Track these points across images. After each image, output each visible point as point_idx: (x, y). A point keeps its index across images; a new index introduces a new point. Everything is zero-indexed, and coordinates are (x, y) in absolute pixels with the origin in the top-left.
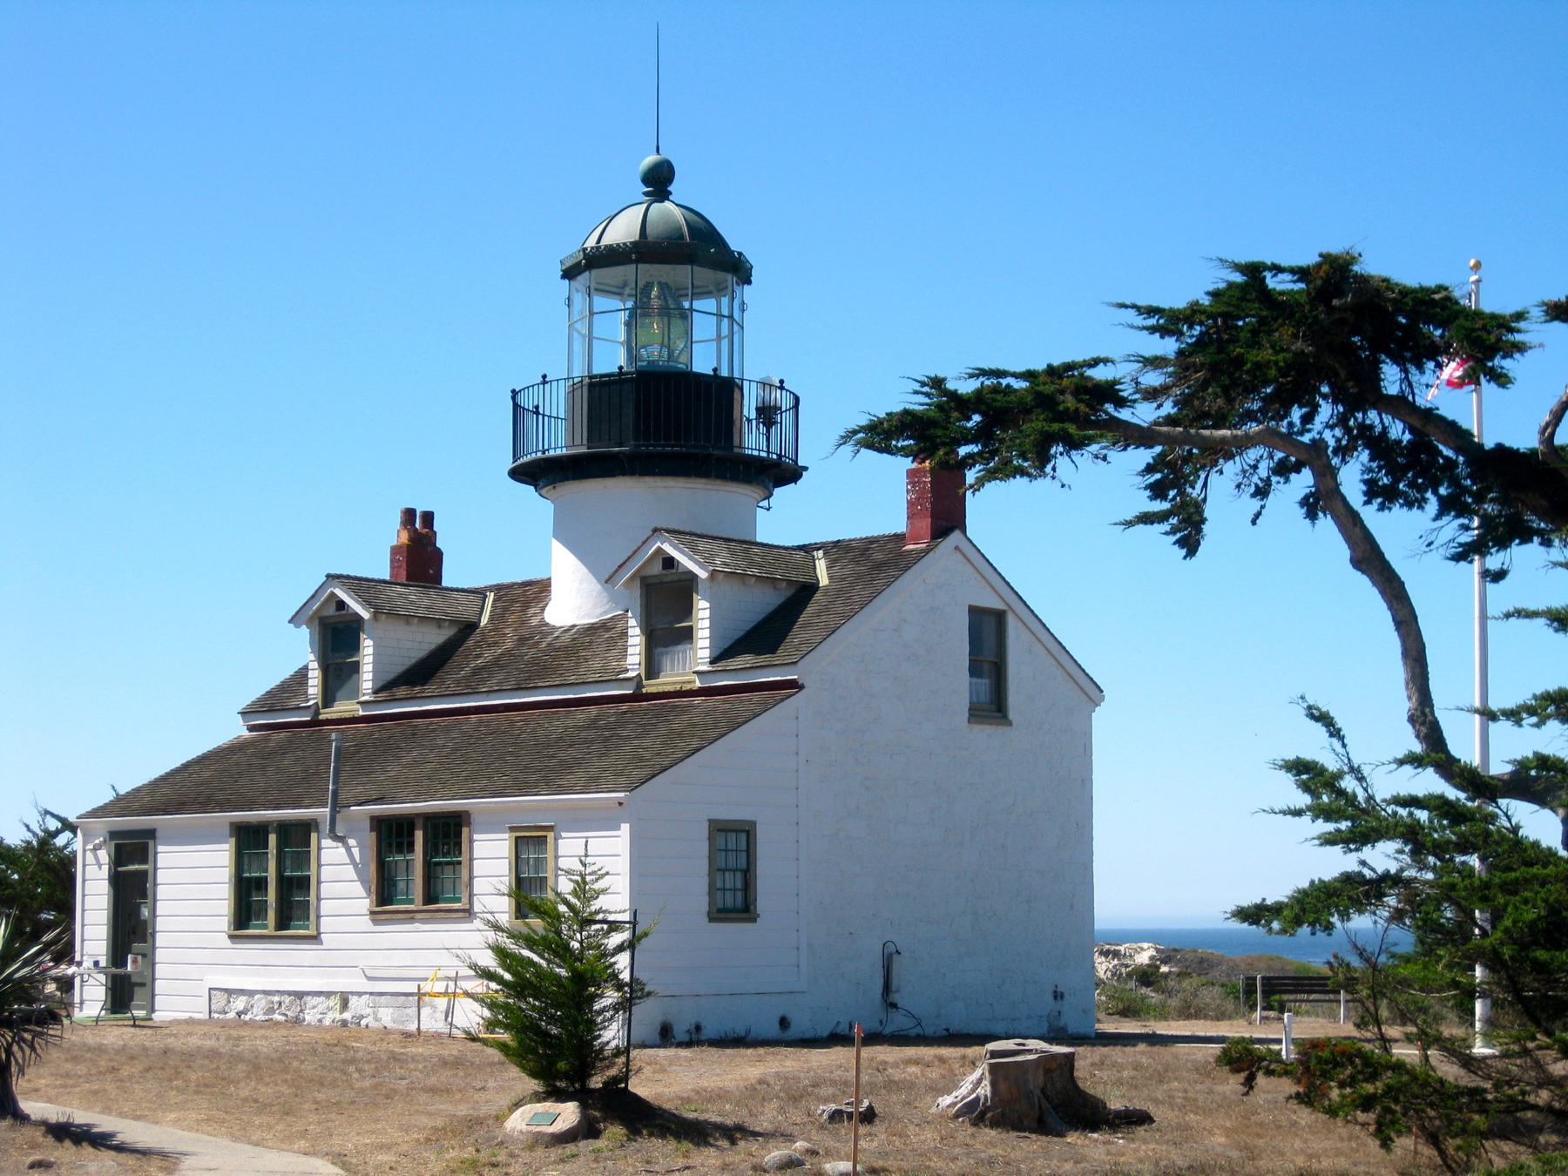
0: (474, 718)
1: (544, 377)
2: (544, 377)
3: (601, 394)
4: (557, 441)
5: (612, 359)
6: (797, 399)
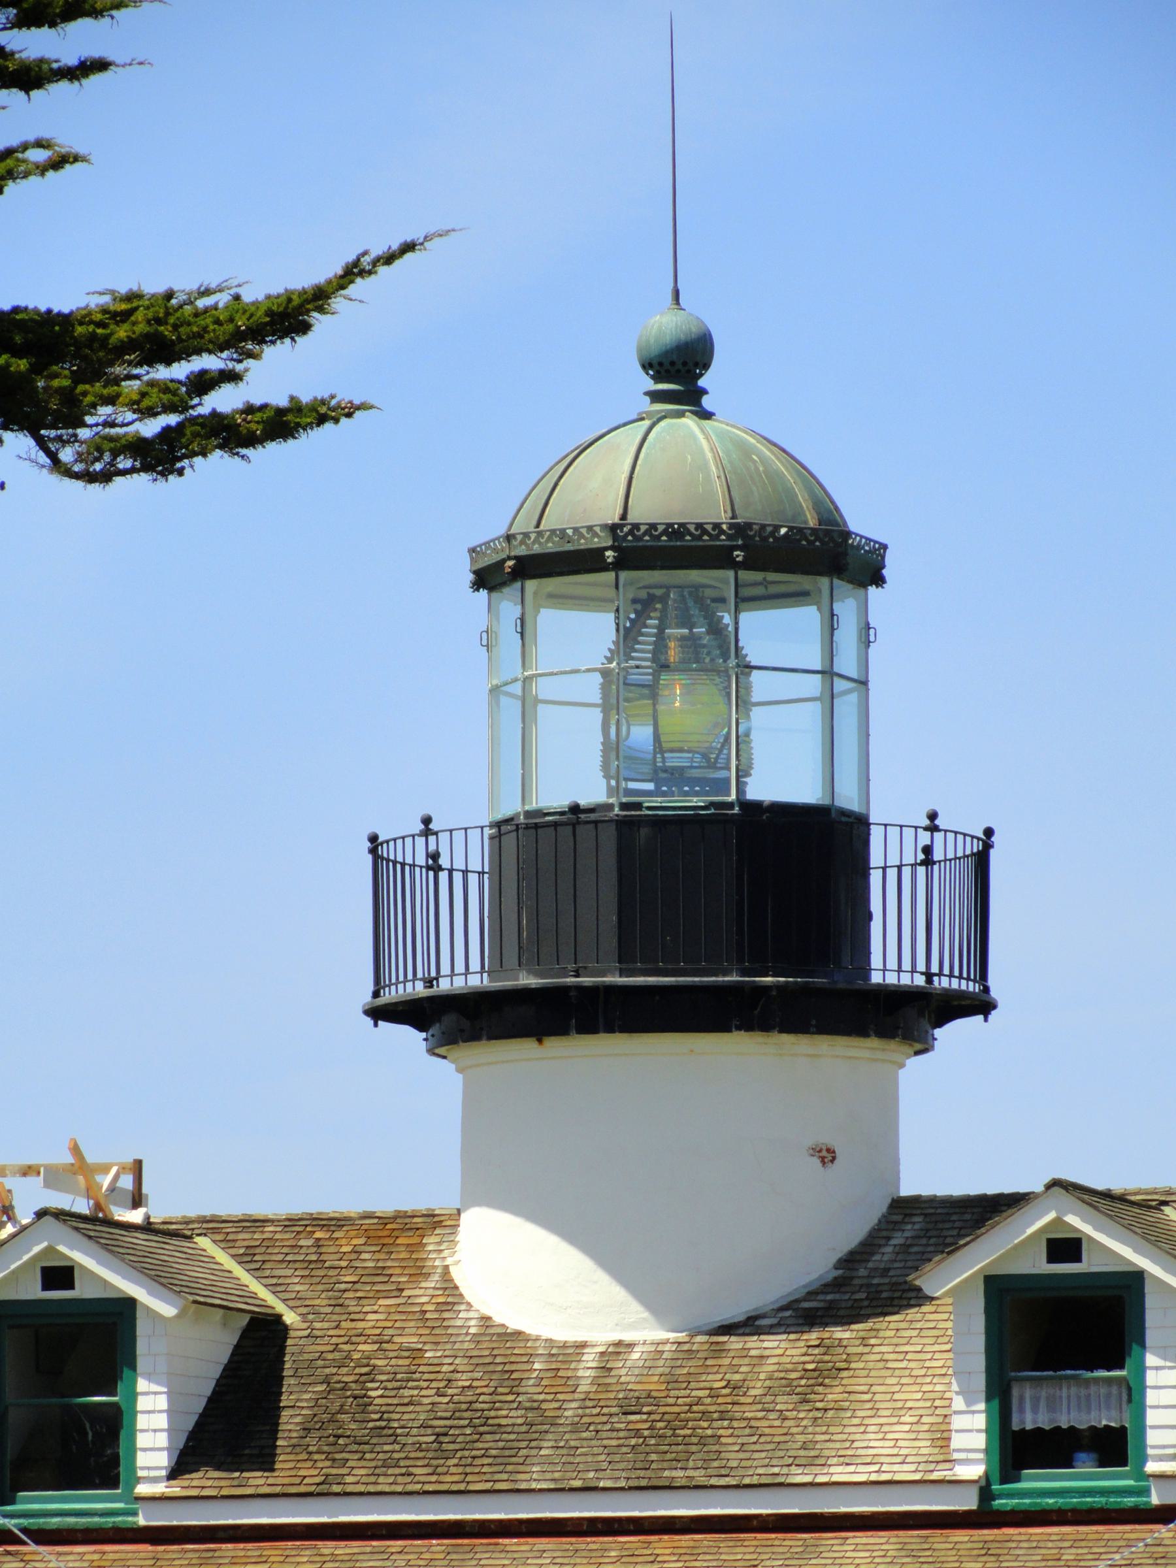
1: (427, 821)
5: (574, 774)
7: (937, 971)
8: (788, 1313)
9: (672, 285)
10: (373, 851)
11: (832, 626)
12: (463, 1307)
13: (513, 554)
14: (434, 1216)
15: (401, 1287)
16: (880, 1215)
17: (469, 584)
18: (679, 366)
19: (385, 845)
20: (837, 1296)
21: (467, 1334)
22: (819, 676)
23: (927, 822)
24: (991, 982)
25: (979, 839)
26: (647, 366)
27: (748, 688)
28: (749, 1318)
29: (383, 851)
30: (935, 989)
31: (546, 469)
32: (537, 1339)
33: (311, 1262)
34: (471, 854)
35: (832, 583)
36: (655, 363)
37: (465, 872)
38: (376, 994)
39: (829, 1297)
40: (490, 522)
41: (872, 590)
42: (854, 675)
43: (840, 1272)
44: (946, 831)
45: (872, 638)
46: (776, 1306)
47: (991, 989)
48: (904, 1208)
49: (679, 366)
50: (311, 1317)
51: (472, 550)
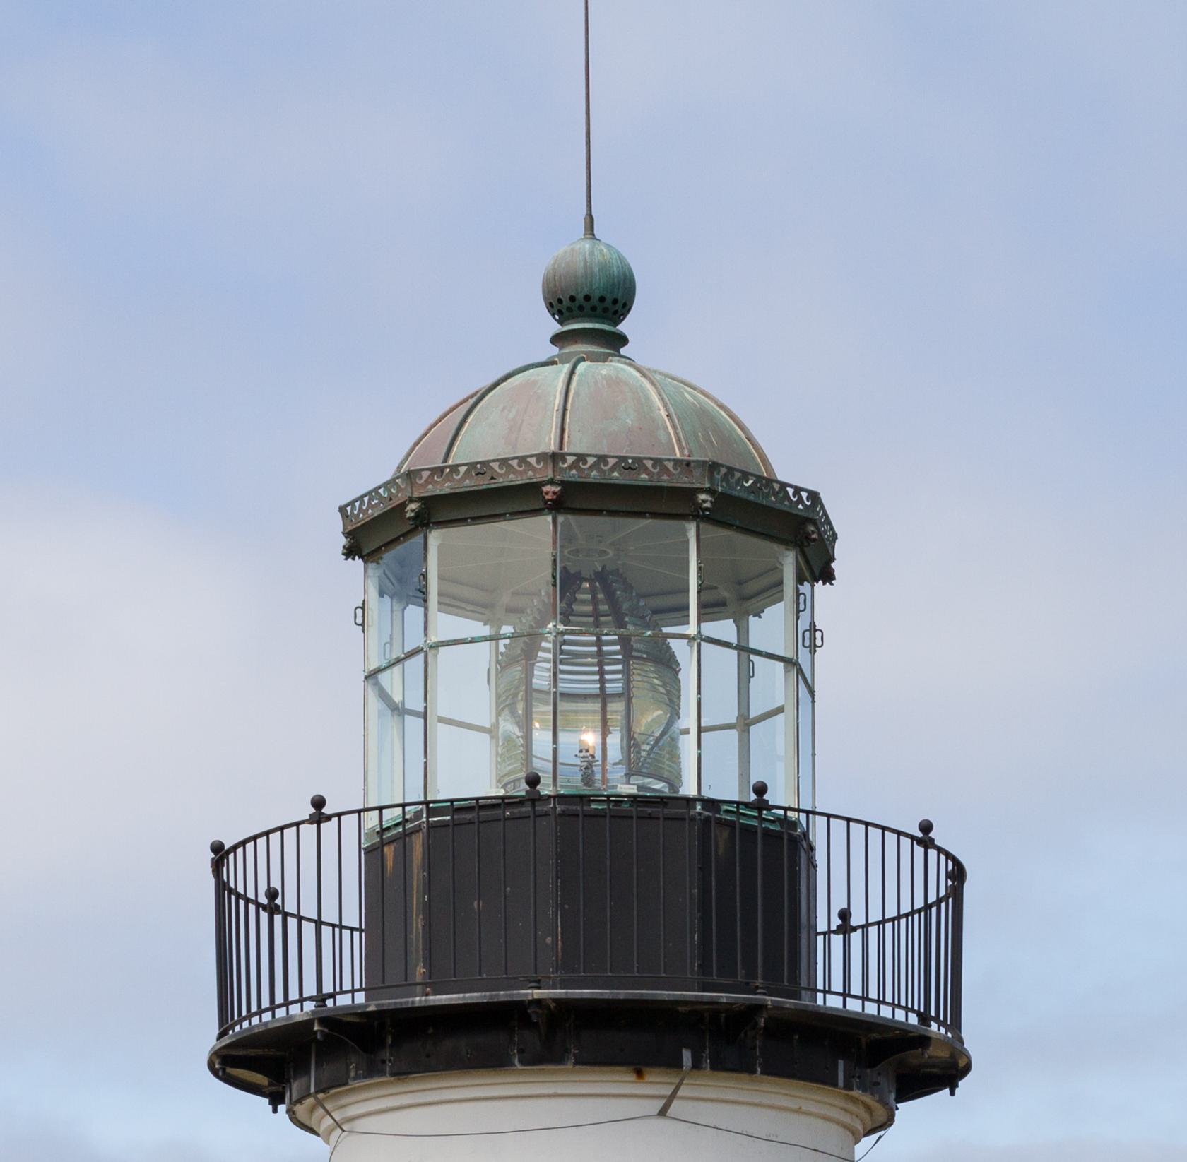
0: (759, 530)
1: (319, 803)
2: (319, 803)
3: (440, 862)
4: (327, 970)
5: (470, 771)
6: (958, 874)
9: (584, 212)
13: (416, 495)
18: (594, 302)
22: (782, 664)
24: (965, 1033)
31: (446, 408)
37: (319, 923)
38: (222, 1035)
40: (371, 463)
41: (819, 586)
45: (818, 642)
49: (608, 303)
51: (342, 510)
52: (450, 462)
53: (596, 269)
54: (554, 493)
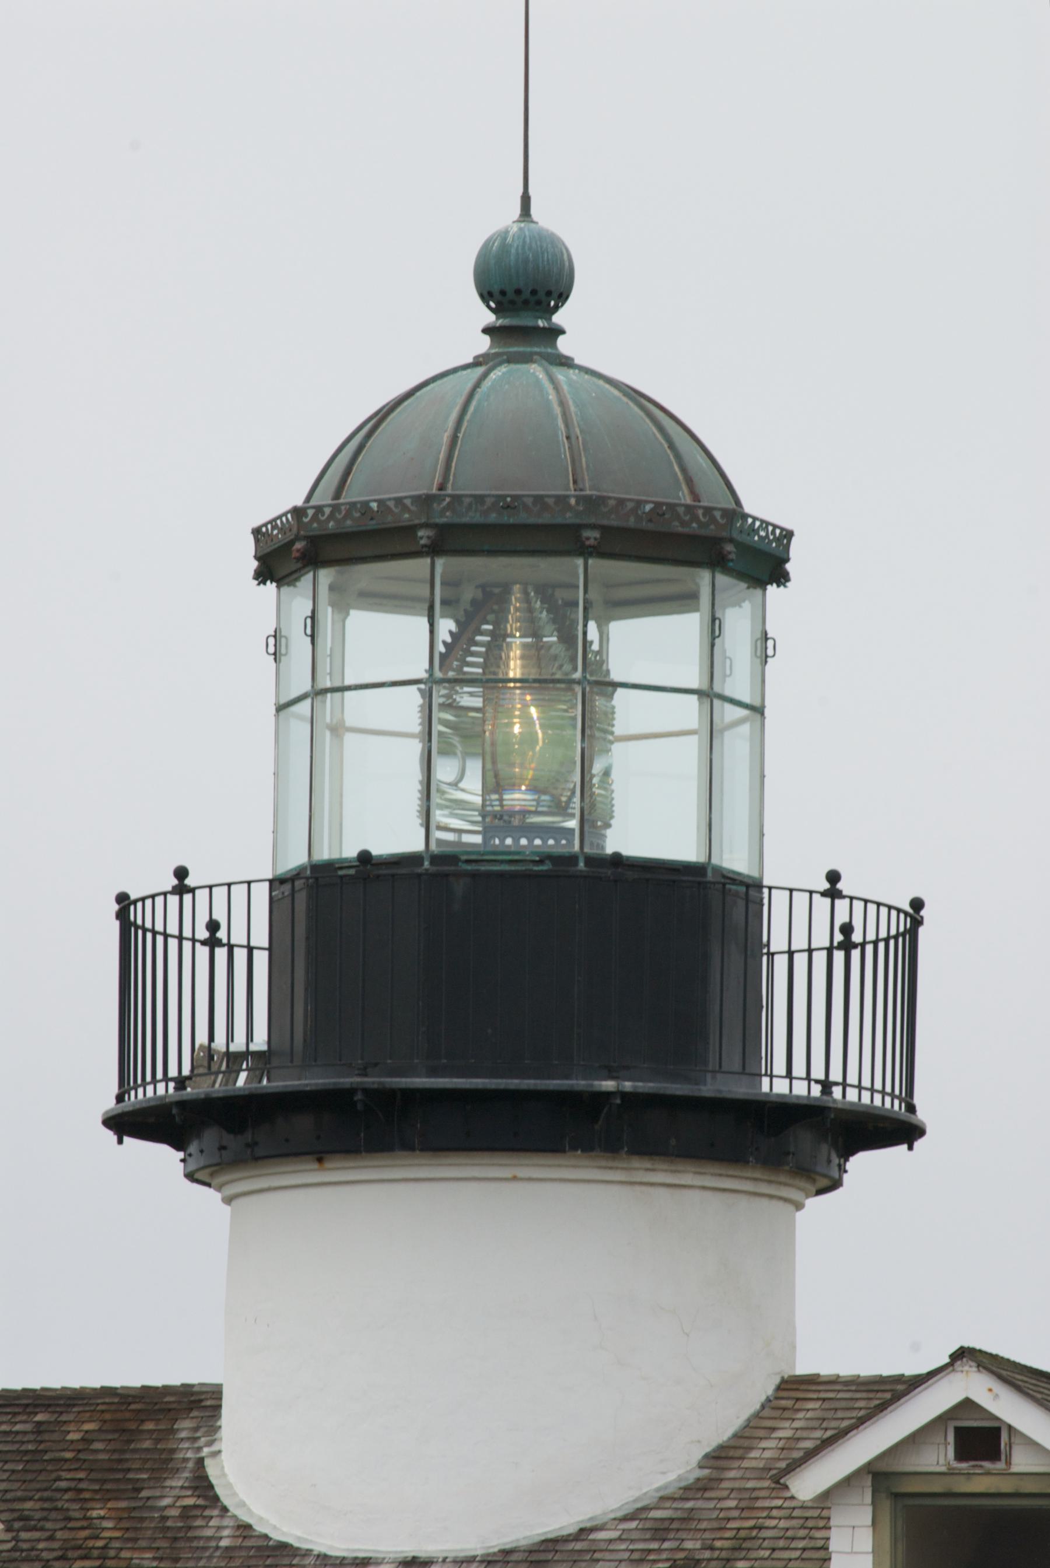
1: (181, 873)
2: (181, 873)
3: (339, 915)
5: (382, 819)
7: (840, 1079)
8: (633, 1525)
10: (122, 915)
11: (713, 631)
12: (216, 1512)
14: (192, 1394)
15: (138, 1485)
16: (763, 1398)
17: (251, 573)
19: (139, 905)
20: (699, 1504)
21: (217, 1548)
22: (695, 697)
23: (826, 885)
25: (906, 914)
26: (486, 296)
27: (610, 715)
28: (582, 1530)
29: (136, 914)
30: (835, 1101)
32: (308, 1552)
33: (26, 1452)
34: (252, 922)
35: (713, 578)
36: (496, 289)
38: (120, 1099)
39: (689, 1505)
40: (286, 486)
41: (772, 589)
42: (746, 699)
43: (706, 1472)
44: (852, 898)
46: (620, 1514)
47: (917, 1108)
48: (795, 1389)
50: (17, 1525)
51: (256, 532)
52: (312, 503)
53: (493, 262)
54: (428, 537)
